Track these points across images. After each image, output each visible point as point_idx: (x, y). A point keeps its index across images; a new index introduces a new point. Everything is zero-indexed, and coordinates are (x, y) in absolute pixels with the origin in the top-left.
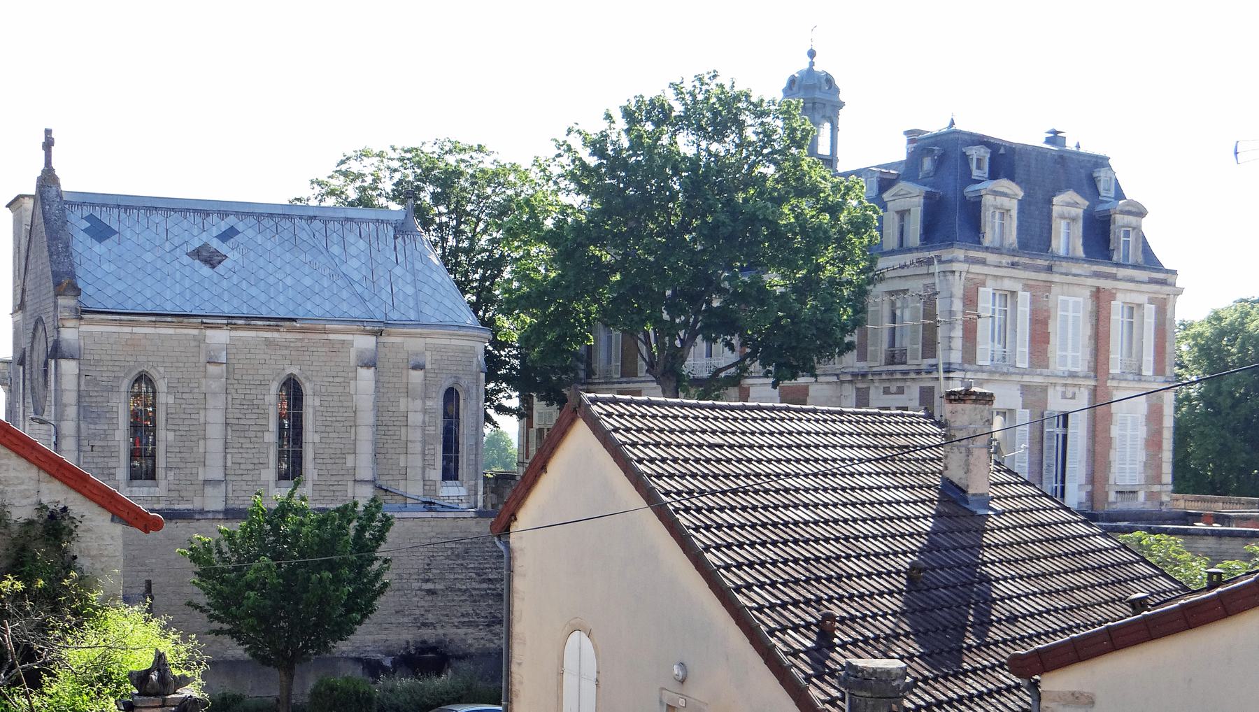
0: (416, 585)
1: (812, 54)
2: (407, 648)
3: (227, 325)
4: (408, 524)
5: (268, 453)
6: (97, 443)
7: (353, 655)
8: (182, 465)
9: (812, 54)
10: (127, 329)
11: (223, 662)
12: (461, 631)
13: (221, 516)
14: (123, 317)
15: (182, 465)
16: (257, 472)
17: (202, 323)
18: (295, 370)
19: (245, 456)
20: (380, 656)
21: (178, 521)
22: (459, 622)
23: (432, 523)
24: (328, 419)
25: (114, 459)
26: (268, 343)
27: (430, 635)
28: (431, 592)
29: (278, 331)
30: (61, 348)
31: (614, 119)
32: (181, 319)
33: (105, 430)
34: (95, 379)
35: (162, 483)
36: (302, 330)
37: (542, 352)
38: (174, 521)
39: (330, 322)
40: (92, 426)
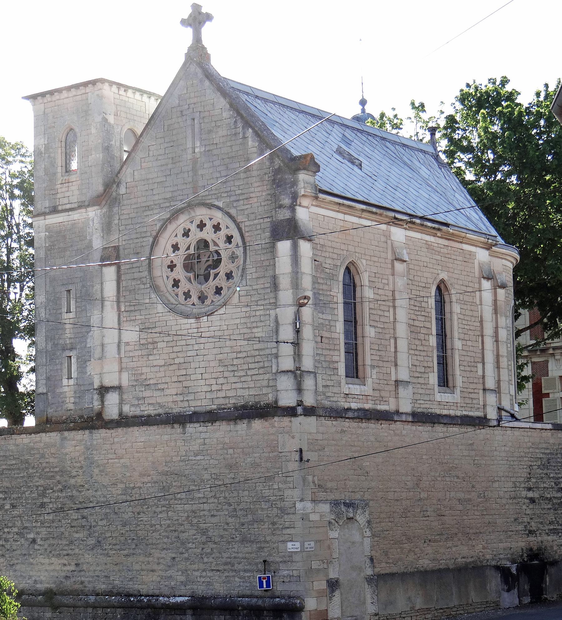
0: (524, 493)
1: (363, 102)
2: (522, 556)
3: (407, 222)
4: (517, 433)
5: (432, 357)
6: (325, 334)
7: (494, 563)
8: (381, 364)
9: (363, 102)
10: (340, 216)
11: (417, 572)
12: (550, 538)
13: (410, 419)
14: (346, 202)
15: (381, 364)
16: (426, 375)
17: (395, 218)
18: (443, 275)
19: (419, 358)
20: (508, 564)
21: (383, 422)
22: (549, 530)
23: (529, 434)
24: (466, 327)
25: (414, 347)
26: (428, 246)
27: (534, 541)
28: (532, 500)
29: (435, 235)
30: (300, 223)
31: (425, 109)
32: (382, 211)
33: (330, 321)
34: (321, 264)
35: (369, 381)
36: (449, 237)
37: (25, 326)
38: (380, 422)
39: (470, 232)
40: (320, 315)
